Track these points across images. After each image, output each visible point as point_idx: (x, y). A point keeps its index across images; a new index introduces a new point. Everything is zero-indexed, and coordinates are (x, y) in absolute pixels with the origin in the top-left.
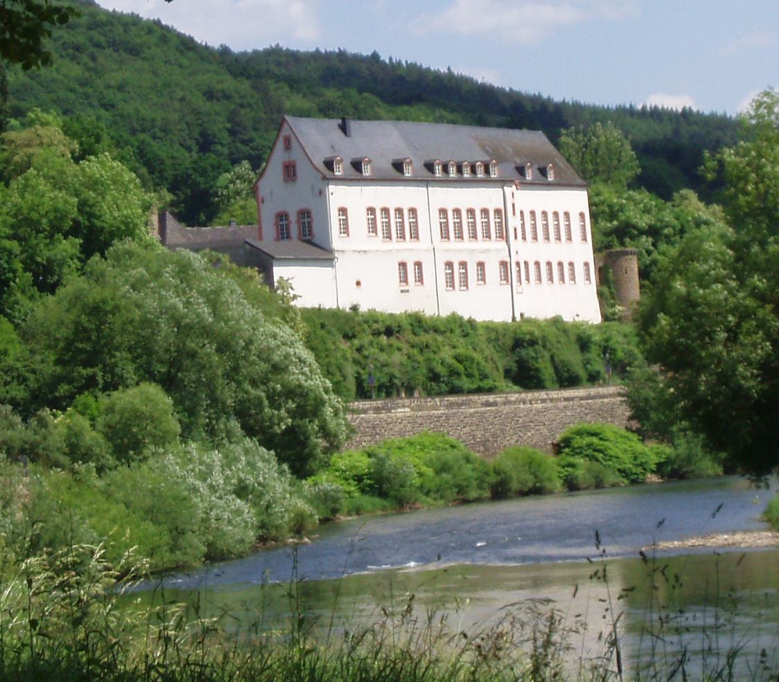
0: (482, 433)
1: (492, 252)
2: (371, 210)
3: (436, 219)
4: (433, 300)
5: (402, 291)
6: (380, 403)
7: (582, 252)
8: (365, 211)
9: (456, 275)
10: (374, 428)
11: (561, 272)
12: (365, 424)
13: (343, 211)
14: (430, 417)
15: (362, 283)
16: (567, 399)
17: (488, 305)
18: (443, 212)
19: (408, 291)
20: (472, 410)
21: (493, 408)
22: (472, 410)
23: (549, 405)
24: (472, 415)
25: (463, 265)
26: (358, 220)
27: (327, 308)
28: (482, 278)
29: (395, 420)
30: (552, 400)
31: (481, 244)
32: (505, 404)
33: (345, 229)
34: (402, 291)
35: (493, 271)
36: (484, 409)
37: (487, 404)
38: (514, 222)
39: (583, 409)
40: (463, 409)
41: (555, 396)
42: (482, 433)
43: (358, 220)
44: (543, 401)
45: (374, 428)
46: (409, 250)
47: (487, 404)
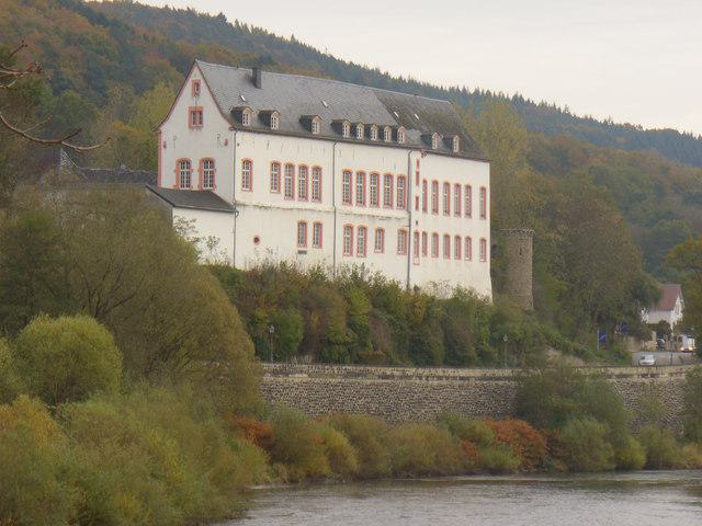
1: (391, 219)
2: (275, 165)
7: (479, 228)
8: (269, 165)
11: (456, 247)
13: (247, 163)
15: (252, 239)
16: (461, 378)
23: (444, 382)
24: (368, 387)
25: (363, 229)
26: (262, 175)
28: (380, 246)
30: (447, 378)
32: (401, 378)
35: (391, 240)
36: (380, 381)
40: (359, 379)
43: (262, 175)
44: (440, 378)
45: (270, 391)
46: (310, 211)
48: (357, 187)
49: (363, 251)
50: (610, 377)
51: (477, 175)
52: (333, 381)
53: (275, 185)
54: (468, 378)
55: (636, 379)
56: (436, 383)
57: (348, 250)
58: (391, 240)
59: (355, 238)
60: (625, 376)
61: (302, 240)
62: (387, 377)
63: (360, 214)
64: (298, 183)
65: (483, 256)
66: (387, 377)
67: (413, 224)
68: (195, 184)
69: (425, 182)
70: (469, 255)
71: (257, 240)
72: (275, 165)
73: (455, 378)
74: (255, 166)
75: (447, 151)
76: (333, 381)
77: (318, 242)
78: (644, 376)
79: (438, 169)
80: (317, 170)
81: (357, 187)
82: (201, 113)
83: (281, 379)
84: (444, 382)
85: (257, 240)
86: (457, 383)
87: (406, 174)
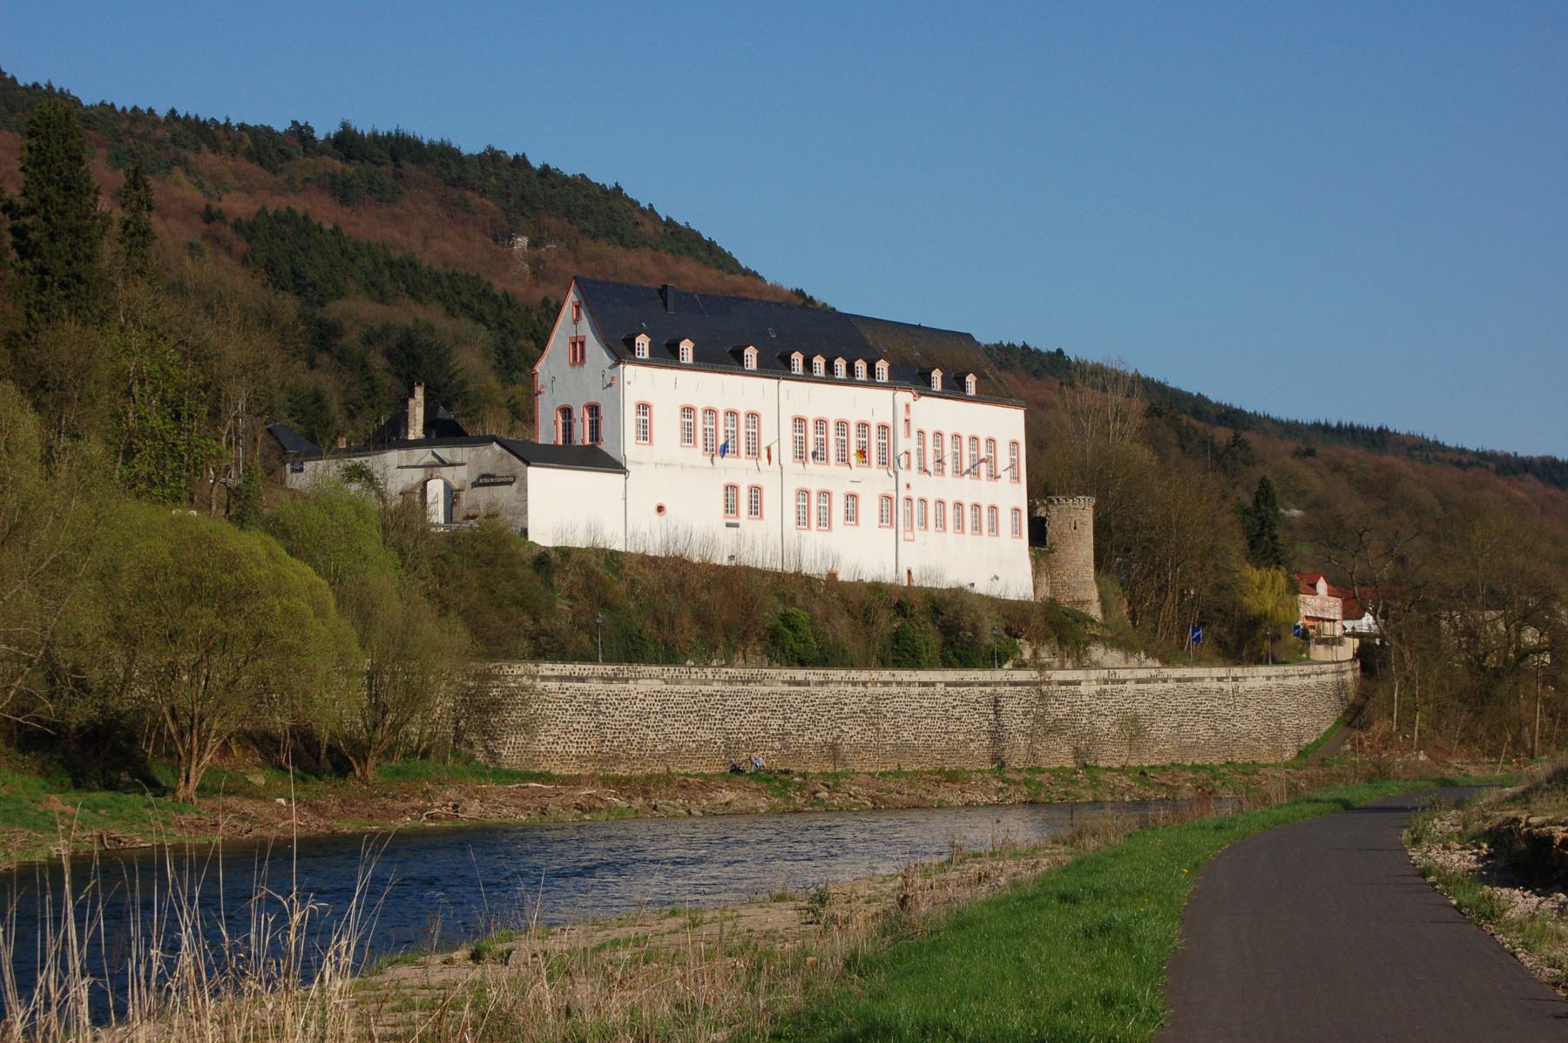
0: (781, 722)
1: (872, 482)
2: (688, 410)
3: (676, 419)
4: (764, 542)
5: (728, 525)
6: (609, 669)
7: (1013, 495)
8: (678, 413)
9: (812, 509)
10: (596, 704)
11: (982, 519)
12: (581, 698)
13: (644, 407)
14: (694, 695)
15: (654, 509)
16: (925, 684)
17: (863, 553)
18: (799, 422)
19: (737, 525)
20: (766, 690)
21: (802, 689)
22: (766, 690)
23: (894, 689)
24: (764, 697)
25: (826, 494)
26: (667, 423)
27: (868, 580)
28: (852, 516)
29: (634, 694)
30: (899, 684)
31: (857, 471)
32: (822, 684)
33: (645, 433)
34: (728, 525)
35: (869, 509)
36: (786, 688)
37: (794, 682)
38: (906, 443)
39: (950, 699)
40: (751, 687)
41: (906, 679)
42: (781, 722)
43: (667, 423)
44: (886, 684)
45: (596, 704)
46: (739, 470)
47: (794, 682)
48: (812, 443)
49: (825, 522)
50: (1049, 683)
51: (1005, 425)
52: (705, 689)
53: (688, 435)
54: (933, 684)
55: (1207, 684)
56: (880, 690)
57: (802, 520)
58: (869, 509)
59: (812, 509)
60: (1190, 680)
61: (731, 507)
62: (798, 684)
63: (817, 476)
64: (723, 439)
65: (1016, 532)
66: (798, 684)
67: (902, 486)
68: (582, 435)
69: (921, 432)
70: (994, 529)
71: (660, 509)
72: (688, 410)
73: (910, 684)
74: (603, 412)
75: (954, 389)
76: (705, 689)
77: (756, 509)
78: (1220, 679)
79: (938, 414)
80: (753, 415)
81: (812, 443)
82: (582, 344)
83: (616, 687)
84: (894, 689)
85: (660, 509)
86: (915, 690)
87: (889, 422)
